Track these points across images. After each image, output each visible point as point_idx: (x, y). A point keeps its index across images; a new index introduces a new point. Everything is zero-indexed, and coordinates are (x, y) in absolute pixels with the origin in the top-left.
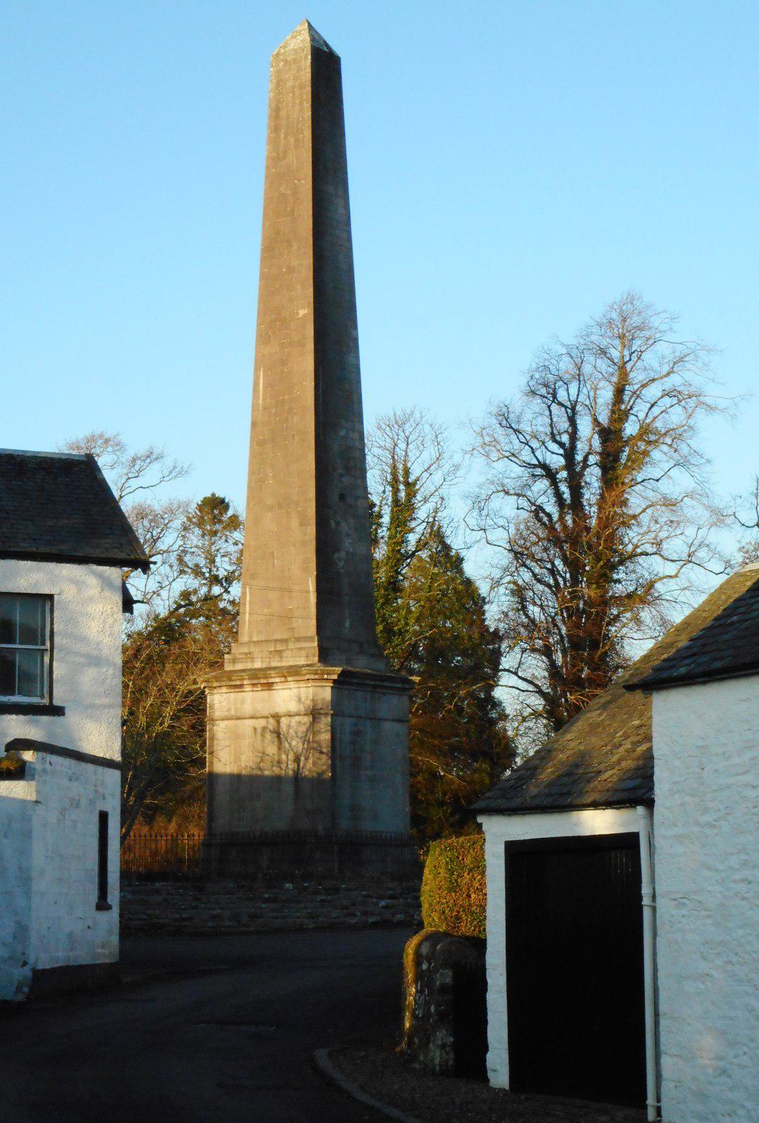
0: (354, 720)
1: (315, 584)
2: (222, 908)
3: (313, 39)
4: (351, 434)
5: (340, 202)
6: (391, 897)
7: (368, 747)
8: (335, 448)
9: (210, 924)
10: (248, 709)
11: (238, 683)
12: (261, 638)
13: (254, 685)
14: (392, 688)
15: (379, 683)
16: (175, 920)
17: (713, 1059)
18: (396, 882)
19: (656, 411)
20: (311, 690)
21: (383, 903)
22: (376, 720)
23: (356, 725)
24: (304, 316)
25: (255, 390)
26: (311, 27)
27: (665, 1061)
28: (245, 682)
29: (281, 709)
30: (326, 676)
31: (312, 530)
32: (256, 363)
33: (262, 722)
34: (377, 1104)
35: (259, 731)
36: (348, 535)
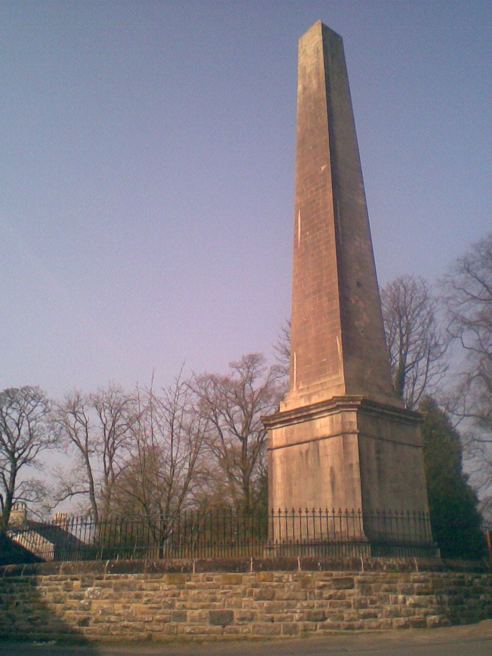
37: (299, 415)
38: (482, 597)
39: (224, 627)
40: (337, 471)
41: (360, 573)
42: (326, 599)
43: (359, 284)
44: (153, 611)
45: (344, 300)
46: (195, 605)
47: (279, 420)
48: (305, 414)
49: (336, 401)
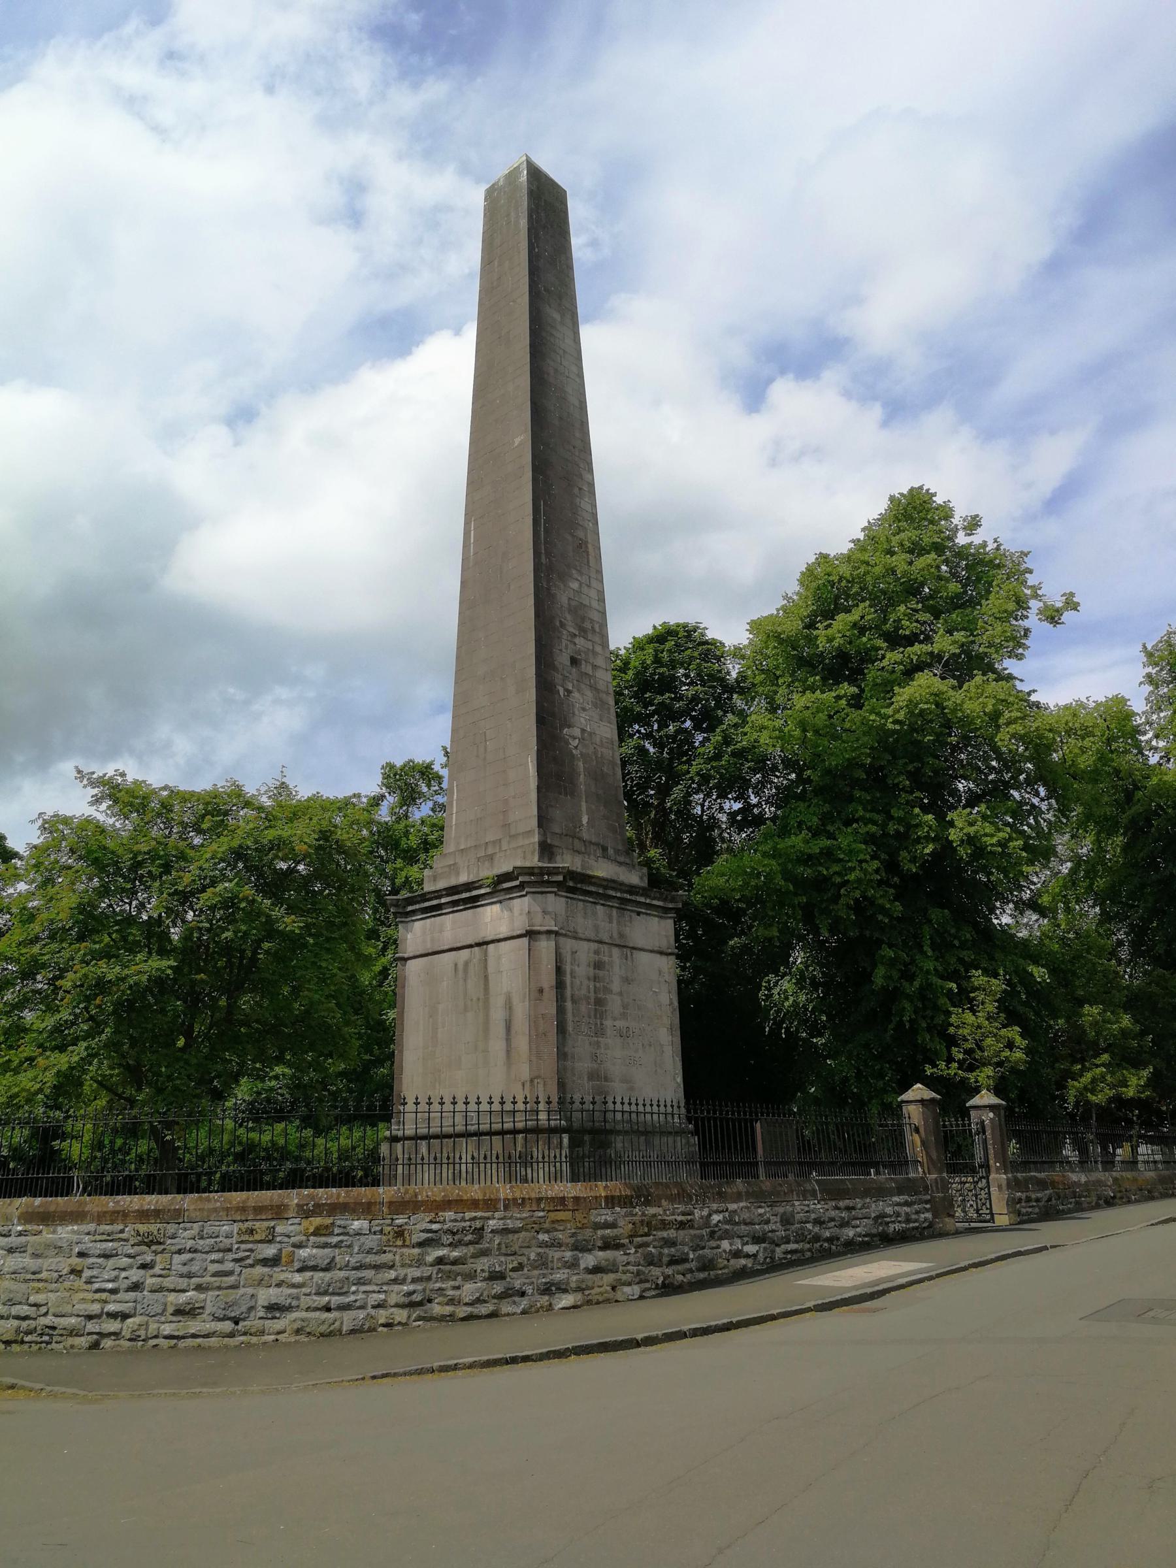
0: (594, 946)
2: (199, 1288)
4: (585, 589)
5: (569, 341)
7: (616, 986)
8: (563, 599)
12: (470, 843)
18: (618, 1209)
21: (589, 1260)
22: (628, 948)
23: (597, 952)
27: (519, 900)
31: (531, 694)
35: (461, 967)
36: (584, 709)
37: (456, 897)
38: (1082, 874)
39: (237, 1323)
40: (516, 1001)
41: (497, 1215)
42: (431, 1265)
43: (574, 661)
44: (104, 1296)
45: (545, 686)
46: (183, 1283)
47: (417, 906)
48: (464, 895)
49: (519, 874)
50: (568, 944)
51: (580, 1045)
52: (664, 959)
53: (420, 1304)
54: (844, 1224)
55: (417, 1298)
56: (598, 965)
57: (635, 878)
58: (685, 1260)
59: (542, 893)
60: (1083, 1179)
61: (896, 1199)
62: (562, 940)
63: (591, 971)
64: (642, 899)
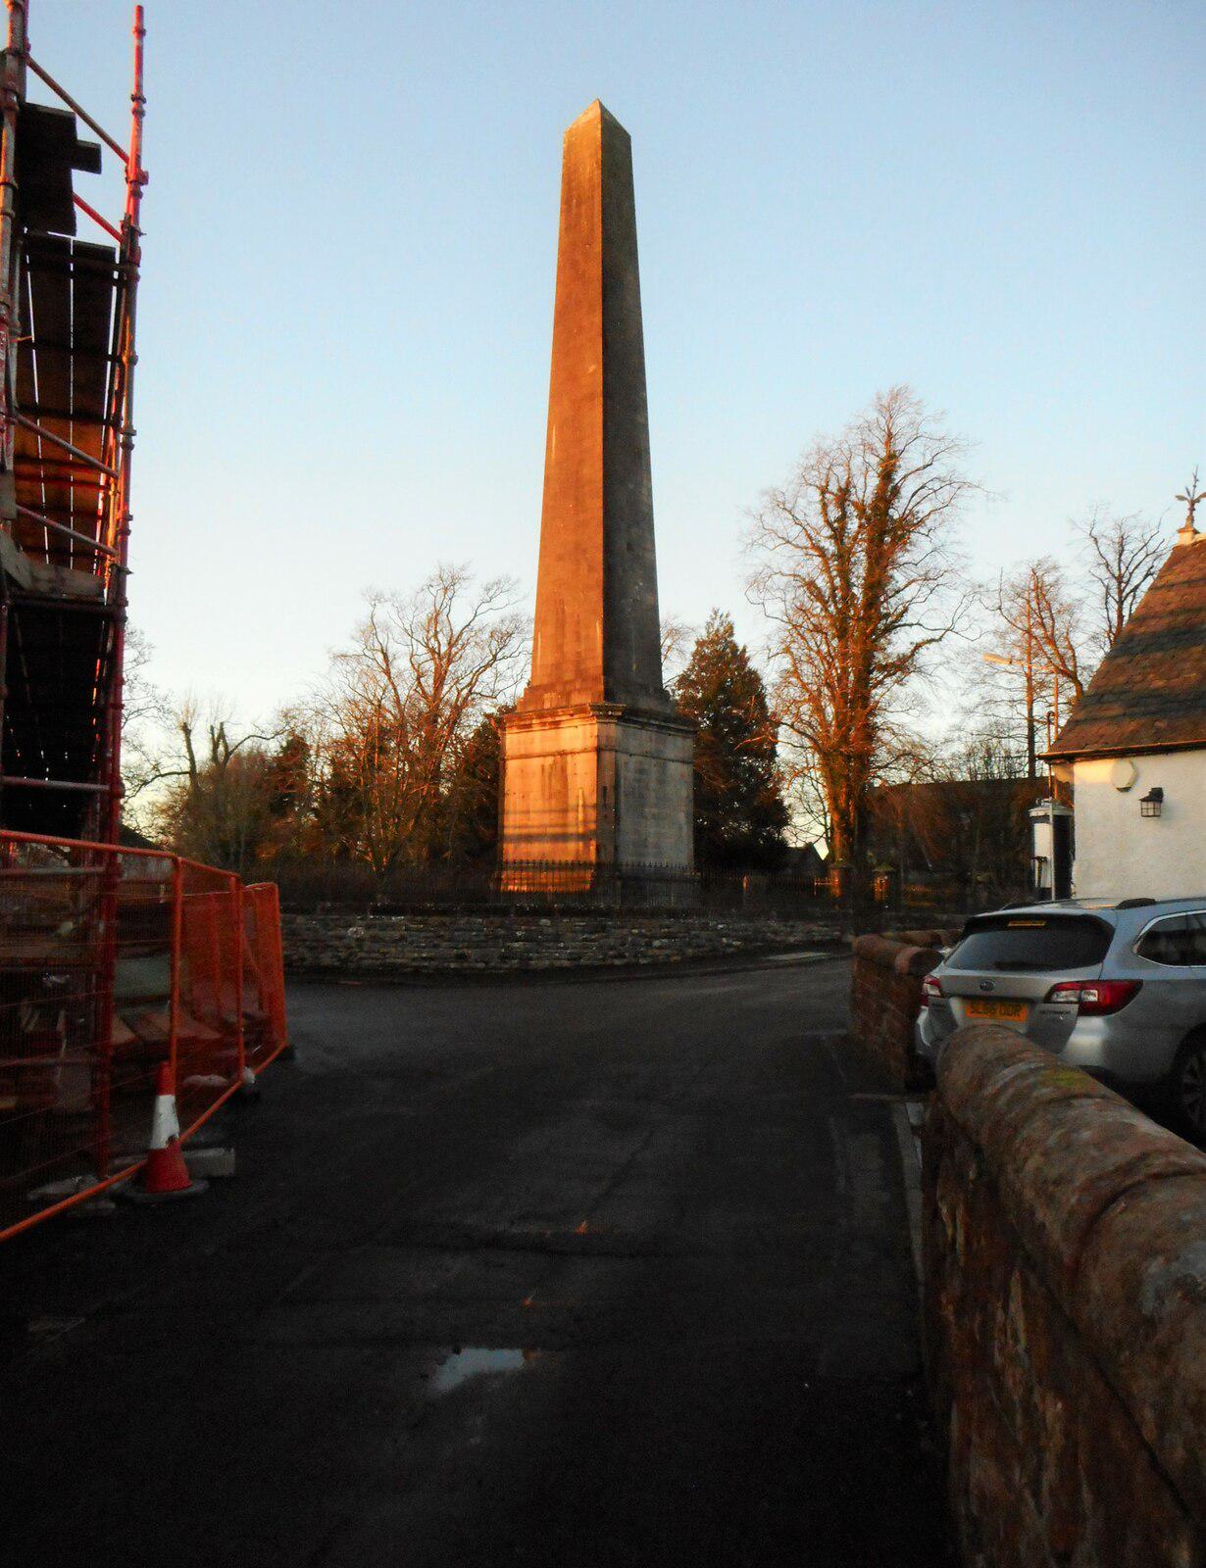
1: (601, 626)
3: (602, 113)
6: (668, 936)
7: (653, 785)
9: (452, 965)
10: (537, 748)
11: (528, 722)
13: (544, 724)
14: (679, 730)
15: (663, 724)
16: (414, 959)
17: (555, 811)
19: (916, 499)
20: (596, 726)
24: (595, 371)
25: (549, 448)
26: (601, 104)
28: (534, 721)
29: (566, 746)
30: (610, 713)
32: (549, 422)
33: (549, 760)
34: (926, 856)
43: (630, 547)
50: (623, 758)
51: (627, 823)
52: (685, 766)
53: (575, 959)
54: (791, 934)
55: (574, 956)
56: (641, 771)
57: (1018, 1056)
58: (704, 946)
59: (607, 723)
60: (922, 903)
61: (821, 923)
62: (619, 754)
63: (637, 776)
64: (673, 726)
